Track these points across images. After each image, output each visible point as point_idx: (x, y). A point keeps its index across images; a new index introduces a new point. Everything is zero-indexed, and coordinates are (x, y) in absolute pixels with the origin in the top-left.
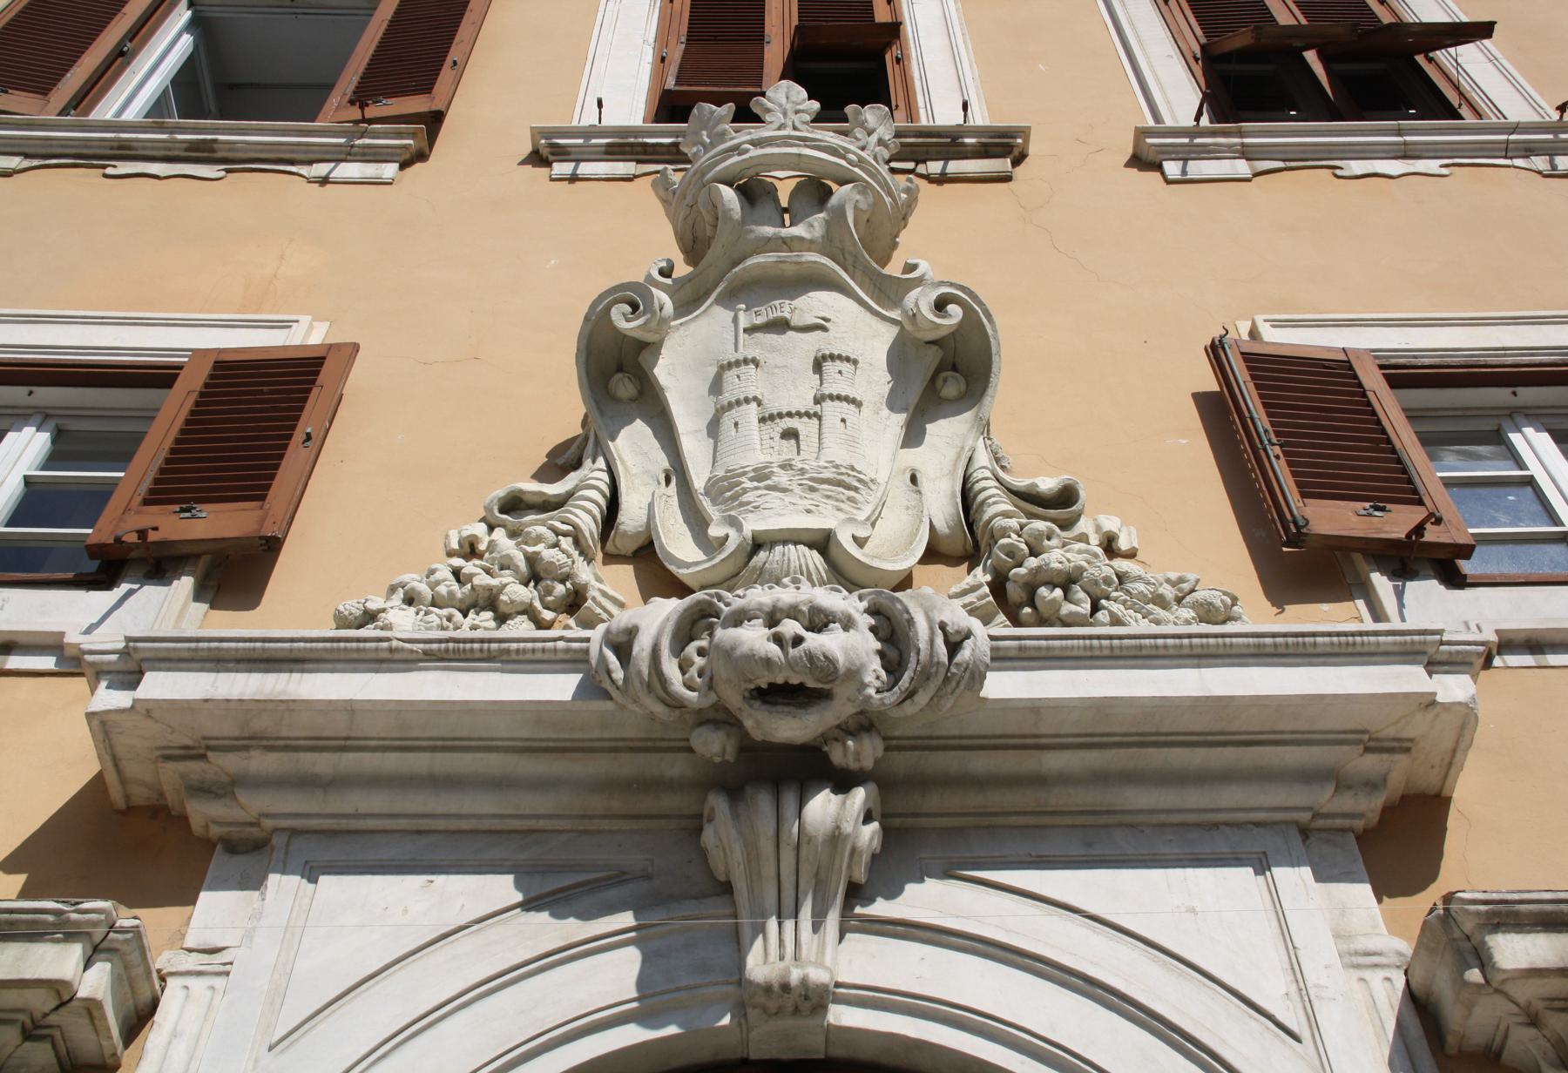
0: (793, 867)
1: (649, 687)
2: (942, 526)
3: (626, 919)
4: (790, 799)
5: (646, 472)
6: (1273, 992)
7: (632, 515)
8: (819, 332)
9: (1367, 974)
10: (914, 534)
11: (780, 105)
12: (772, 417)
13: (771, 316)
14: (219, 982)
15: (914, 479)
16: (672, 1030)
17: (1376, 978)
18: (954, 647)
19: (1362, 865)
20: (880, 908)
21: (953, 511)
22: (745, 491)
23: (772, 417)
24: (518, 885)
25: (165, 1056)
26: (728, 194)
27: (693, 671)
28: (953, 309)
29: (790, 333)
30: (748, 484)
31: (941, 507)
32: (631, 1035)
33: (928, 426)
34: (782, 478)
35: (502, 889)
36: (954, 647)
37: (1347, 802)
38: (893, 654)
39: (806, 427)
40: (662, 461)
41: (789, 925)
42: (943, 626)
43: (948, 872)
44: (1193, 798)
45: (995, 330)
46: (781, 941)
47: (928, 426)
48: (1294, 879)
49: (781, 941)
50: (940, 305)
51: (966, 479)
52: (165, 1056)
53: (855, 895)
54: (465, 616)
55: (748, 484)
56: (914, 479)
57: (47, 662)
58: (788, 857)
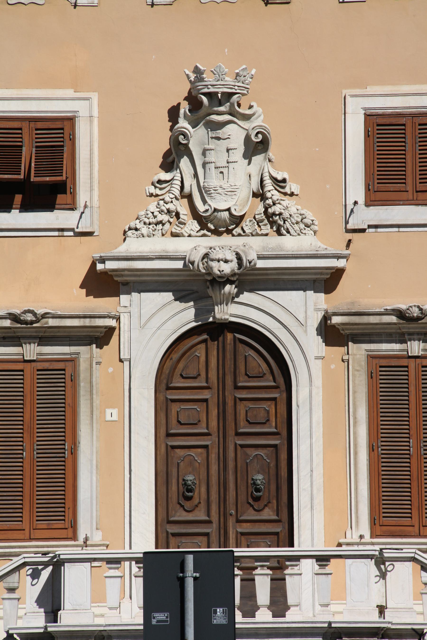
0: (233, 417)
1: (197, 270)
2: (255, 190)
3: (192, 303)
4: (222, 287)
5: (189, 173)
6: (301, 318)
7: (187, 189)
8: (228, 139)
9: (318, 312)
10: (250, 192)
11: (218, 73)
12: (217, 168)
13: (217, 136)
14: (342, 541)
15: (250, 176)
16: (200, 323)
17: (319, 313)
18: (250, 263)
19: (323, 288)
20: (236, 300)
21: (257, 186)
22: (212, 193)
23: (217, 168)
24: (173, 295)
25: (124, 328)
26: (205, 100)
27: (205, 266)
28: (260, 136)
29: (221, 140)
30: (213, 192)
31: (255, 186)
32: (194, 324)
33: (245, 292)
34: (220, 190)
35: (169, 296)
36: (250, 263)
37: (323, 276)
38: (240, 262)
39: (225, 171)
40: (193, 172)
41: (222, 305)
42: (248, 260)
43: (251, 291)
44: (294, 277)
45: (270, 136)
46: (221, 308)
47: (245, 292)
48: (310, 293)
49: (221, 308)
50: (256, 135)
51: (262, 174)
52: (124, 328)
53: (231, 299)
54: (156, 226)
55: (213, 192)
56: (250, 176)
57: (71, 234)
58: (222, 296)
